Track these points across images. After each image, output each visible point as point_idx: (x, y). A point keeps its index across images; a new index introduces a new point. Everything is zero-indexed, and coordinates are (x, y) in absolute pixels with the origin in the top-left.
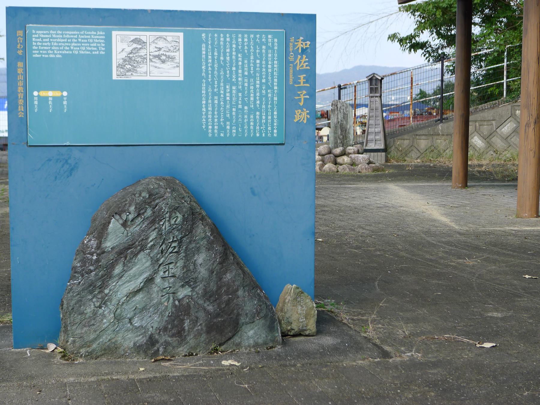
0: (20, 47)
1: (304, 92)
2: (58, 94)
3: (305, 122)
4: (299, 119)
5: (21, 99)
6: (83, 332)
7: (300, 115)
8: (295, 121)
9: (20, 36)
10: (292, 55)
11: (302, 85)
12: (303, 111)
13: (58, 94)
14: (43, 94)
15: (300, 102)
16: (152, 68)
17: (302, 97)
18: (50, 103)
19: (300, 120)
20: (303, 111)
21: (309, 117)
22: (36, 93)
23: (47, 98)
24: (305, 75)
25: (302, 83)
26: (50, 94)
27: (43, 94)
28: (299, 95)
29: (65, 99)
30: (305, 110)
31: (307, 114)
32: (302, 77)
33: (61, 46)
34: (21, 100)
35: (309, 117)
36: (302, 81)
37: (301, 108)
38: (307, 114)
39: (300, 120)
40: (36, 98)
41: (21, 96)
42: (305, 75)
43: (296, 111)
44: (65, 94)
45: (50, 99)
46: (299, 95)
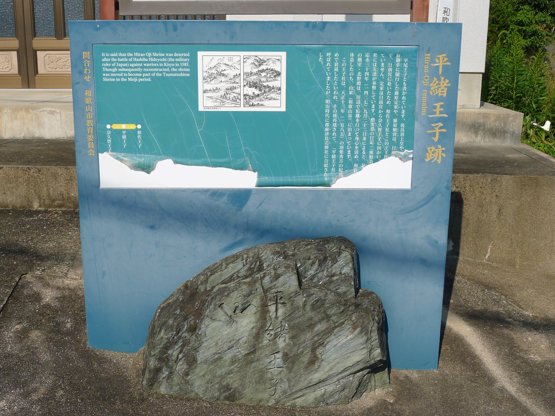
0: (88, 71)
1: (441, 124)
2: (132, 127)
3: (439, 161)
4: (431, 158)
5: (90, 134)
6: (185, 323)
7: (433, 153)
8: (427, 160)
9: (87, 58)
10: (426, 78)
11: (438, 115)
12: (437, 148)
13: (132, 127)
14: (116, 127)
15: (435, 136)
16: (238, 67)
17: (437, 131)
18: (124, 137)
19: (432, 159)
20: (437, 148)
21: (444, 155)
22: (108, 126)
23: (120, 131)
24: (442, 103)
25: (438, 113)
26: (124, 126)
27: (116, 127)
28: (433, 128)
29: (520, 28)
30: (439, 146)
31: (443, 151)
32: (438, 105)
33: (113, 62)
34: (90, 136)
35: (444, 155)
36: (438, 110)
37: (435, 145)
38: (443, 151)
39: (432, 159)
40: (109, 133)
41: (90, 130)
42: (442, 103)
43: (429, 149)
44: (139, 127)
45: (124, 132)
46: (433, 128)
